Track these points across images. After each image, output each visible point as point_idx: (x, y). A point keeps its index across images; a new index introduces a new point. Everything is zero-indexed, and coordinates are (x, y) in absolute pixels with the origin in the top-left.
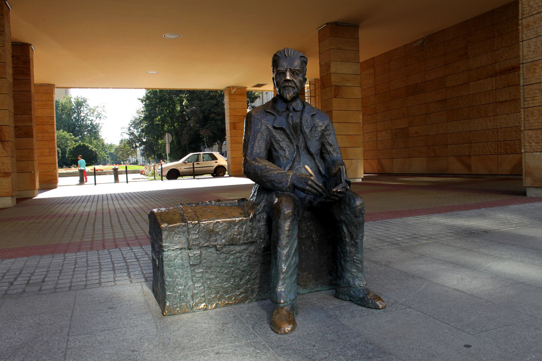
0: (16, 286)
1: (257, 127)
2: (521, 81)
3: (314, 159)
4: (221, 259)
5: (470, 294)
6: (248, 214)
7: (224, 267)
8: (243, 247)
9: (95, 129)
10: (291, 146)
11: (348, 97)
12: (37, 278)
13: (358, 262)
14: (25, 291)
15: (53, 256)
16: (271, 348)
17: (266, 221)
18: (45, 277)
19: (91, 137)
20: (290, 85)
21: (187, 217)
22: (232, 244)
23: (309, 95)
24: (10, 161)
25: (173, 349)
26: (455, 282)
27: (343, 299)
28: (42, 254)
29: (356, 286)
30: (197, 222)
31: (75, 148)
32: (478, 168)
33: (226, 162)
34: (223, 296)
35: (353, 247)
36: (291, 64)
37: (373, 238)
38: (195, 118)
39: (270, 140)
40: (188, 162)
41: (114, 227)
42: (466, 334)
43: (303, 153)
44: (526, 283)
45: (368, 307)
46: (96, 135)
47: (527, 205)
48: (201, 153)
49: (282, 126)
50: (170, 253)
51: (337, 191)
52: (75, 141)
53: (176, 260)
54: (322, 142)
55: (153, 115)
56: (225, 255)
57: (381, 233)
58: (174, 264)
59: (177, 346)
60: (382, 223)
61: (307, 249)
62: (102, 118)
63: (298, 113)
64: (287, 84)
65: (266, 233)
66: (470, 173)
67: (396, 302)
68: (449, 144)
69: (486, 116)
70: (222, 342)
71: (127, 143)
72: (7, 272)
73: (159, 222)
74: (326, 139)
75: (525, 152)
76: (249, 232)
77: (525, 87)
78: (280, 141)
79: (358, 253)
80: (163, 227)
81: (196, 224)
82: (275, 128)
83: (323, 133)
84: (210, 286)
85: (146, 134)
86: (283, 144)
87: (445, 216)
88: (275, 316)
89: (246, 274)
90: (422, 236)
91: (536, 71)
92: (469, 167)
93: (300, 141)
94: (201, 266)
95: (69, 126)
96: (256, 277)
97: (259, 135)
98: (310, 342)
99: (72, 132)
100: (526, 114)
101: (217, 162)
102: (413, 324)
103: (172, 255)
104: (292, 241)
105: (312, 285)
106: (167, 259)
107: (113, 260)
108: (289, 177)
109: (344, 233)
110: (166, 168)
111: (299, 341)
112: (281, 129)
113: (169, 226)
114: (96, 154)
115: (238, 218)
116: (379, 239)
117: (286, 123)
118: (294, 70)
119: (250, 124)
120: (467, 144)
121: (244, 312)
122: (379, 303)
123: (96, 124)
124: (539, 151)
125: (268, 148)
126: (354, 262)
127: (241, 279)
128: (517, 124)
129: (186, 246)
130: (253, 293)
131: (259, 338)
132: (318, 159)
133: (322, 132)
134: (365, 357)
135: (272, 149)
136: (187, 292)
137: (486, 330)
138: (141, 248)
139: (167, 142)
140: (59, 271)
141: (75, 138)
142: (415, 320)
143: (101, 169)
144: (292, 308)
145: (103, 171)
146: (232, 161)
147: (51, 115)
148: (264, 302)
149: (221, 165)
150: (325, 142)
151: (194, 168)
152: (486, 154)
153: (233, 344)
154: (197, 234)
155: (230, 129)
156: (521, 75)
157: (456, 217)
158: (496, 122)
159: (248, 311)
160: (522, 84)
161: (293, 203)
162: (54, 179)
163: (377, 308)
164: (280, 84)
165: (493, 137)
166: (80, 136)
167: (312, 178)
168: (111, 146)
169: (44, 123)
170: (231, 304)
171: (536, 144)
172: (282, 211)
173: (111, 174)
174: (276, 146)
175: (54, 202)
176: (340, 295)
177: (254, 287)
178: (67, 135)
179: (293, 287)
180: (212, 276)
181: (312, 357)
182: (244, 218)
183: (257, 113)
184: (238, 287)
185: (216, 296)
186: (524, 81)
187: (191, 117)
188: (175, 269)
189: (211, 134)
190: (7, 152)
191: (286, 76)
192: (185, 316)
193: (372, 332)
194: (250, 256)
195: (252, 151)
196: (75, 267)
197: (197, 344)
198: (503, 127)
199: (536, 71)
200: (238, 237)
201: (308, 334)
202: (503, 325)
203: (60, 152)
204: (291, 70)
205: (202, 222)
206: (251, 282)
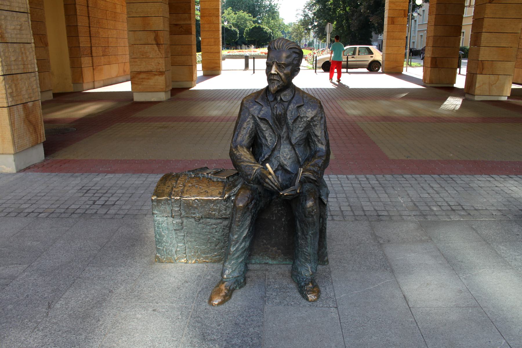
8: (219, 221)
11: (508, 2)
20: (275, 78)
24: (164, 61)
29: (302, 273)
30: (178, 198)
35: (303, 240)
38: (366, 3)
53: (163, 224)
58: (162, 227)
61: (277, 229)
72: (100, 189)
74: (312, 129)
76: (223, 210)
78: (264, 131)
85: (317, 17)
89: (220, 241)
95: (249, 7)
105: (281, 258)
109: (298, 227)
110: (320, 60)
114: (270, 35)
118: (280, 64)
123: (275, 4)
125: (253, 135)
126: (304, 254)
127: (216, 246)
139: (328, 32)
141: (253, 19)
146: (387, 57)
147: (217, 8)
149: (376, 60)
150: (311, 133)
151: (347, 61)
162: (218, 67)
169: (211, 15)
170: (207, 262)
179: (239, 266)
180: (193, 240)
182: (220, 198)
188: (163, 231)
190: (161, 54)
192: (168, 265)
195: (237, 139)
200: (213, 213)
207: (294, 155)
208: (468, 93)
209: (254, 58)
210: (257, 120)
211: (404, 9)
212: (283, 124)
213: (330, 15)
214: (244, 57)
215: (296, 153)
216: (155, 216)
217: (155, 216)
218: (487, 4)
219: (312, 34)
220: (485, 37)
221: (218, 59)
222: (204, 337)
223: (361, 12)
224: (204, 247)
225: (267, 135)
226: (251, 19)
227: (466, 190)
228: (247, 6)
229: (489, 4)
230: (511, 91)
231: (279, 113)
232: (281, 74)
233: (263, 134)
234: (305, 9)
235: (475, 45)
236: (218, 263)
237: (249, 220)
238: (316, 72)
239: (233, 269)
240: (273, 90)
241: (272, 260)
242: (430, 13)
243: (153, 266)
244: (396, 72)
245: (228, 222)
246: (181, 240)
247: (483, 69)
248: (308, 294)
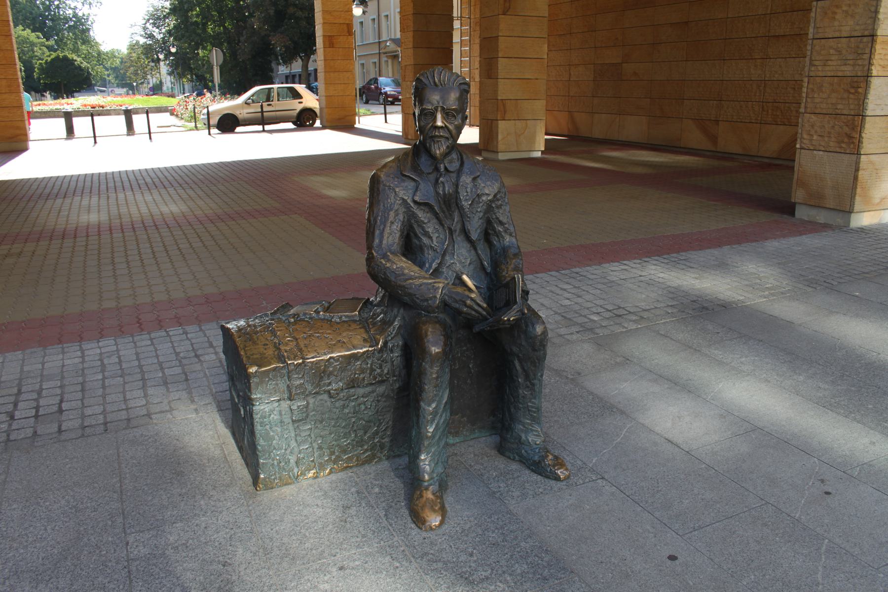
0: (20, 421)
1: (389, 201)
2: (811, 30)
3: (475, 249)
4: (337, 408)
5: (687, 450)
6: (375, 340)
7: (341, 418)
8: (369, 389)
9: (82, 24)
10: (441, 230)
11: (526, 14)
12: (49, 403)
13: (534, 410)
14: (36, 432)
15: (63, 348)
16: (414, 557)
17: (402, 350)
18: (61, 401)
19: (75, 39)
20: (441, 134)
21: (286, 352)
23: (459, 16)
25: (279, 560)
26: (669, 425)
27: (510, 459)
28: (44, 343)
29: (530, 443)
30: (301, 361)
31: (50, 62)
32: (729, 143)
33: (318, 103)
34: (340, 457)
35: (527, 389)
36: (444, 99)
37: (556, 313)
39: (409, 220)
40: (253, 102)
41: (129, 205)
42: (673, 533)
43: (459, 239)
44: (765, 429)
45: (545, 477)
46: (85, 36)
47: (792, 240)
48: (275, 86)
49: (426, 200)
50: (262, 408)
52: (50, 48)
53: (272, 416)
54: (488, 217)
55: (186, 6)
56: (342, 402)
57: (567, 302)
58: (270, 422)
59: (284, 554)
60: (571, 277)
62: (94, 5)
63: (452, 175)
64: (436, 134)
65: (402, 367)
66: (715, 150)
67: (584, 466)
68: (685, 98)
69: (750, 58)
70: (346, 546)
71: (142, 53)
73: (245, 362)
75: (802, 148)
76: (377, 367)
77: (815, 41)
78: (425, 223)
79: (535, 398)
80: (252, 373)
81: (300, 364)
82: (415, 202)
83: (490, 205)
84: (321, 446)
85: (175, 39)
86: (429, 227)
87: (667, 263)
88: (417, 500)
90: (630, 312)
91: (837, 17)
92: (714, 139)
93: (454, 221)
94: (308, 420)
95: (34, 19)
96: (387, 427)
97: (392, 214)
98: (465, 546)
99: (41, 31)
100: (811, 86)
101: (301, 103)
102: (605, 513)
103: (265, 410)
104: (441, 391)
106: (259, 416)
107: (161, 359)
108: (438, 292)
109: (517, 370)
110: (215, 112)
111: (452, 544)
112: (426, 204)
113: (260, 370)
114: (88, 73)
115: (361, 349)
116: (565, 317)
117: (433, 194)
118: (448, 109)
119: (378, 195)
120: (715, 102)
121: (372, 483)
122: (561, 472)
123: (84, 15)
124: (823, 149)
125: (405, 233)
126: (529, 410)
127: (365, 433)
128: (797, 77)
129: (286, 396)
130: (382, 449)
131: (396, 537)
132: (482, 247)
134: (539, 578)
135: (412, 234)
136: (290, 457)
137: (700, 528)
138: (201, 330)
139: (215, 64)
140: (79, 387)
141: (47, 43)
142: (608, 505)
143: (102, 104)
144: (440, 485)
145: (105, 109)
146: (329, 102)
147: (4, 18)
148: (398, 461)
149: (308, 107)
150: (493, 219)
151: (262, 112)
152: (743, 121)
153: (361, 550)
154: (301, 378)
155: (324, 48)
156: (812, 20)
157: (684, 267)
158: (764, 69)
159: (376, 480)
160: (810, 36)
161: (444, 336)
163: (557, 478)
164: (426, 131)
165: (758, 94)
166: (56, 38)
167: (473, 296)
168: (112, 55)
170: (351, 467)
171: (819, 138)
172: (427, 350)
173: (119, 114)
174: (418, 231)
175: (31, 192)
176: (507, 453)
177: (383, 441)
178: (33, 36)
181: (469, 576)
182: (370, 349)
183: (389, 176)
184: (360, 443)
185: (330, 459)
186: (815, 30)
187: (254, 12)
188: (271, 428)
189: (290, 42)
191: (435, 119)
192: (287, 490)
193: (549, 528)
194: (378, 401)
195: (381, 242)
196: (104, 378)
197: (311, 549)
198: (775, 79)
199: (837, 17)
200: (362, 376)
201: (463, 531)
202: (723, 516)
203: (23, 68)
204: (443, 109)
205: (309, 361)
206: (380, 434)
207: (475, 258)
208: (487, 150)
209: (147, 113)
210: (411, 207)
211: (347, 22)
212: (453, 209)
213: (199, 35)
214: (63, 114)
215: (478, 255)
216: (258, 404)
217: (258, 404)
218: (500, 16)
219: (164, 68)
220: (503, 65)
221: (20, 119)
222: (466, 578)
223: (254, 29)
224: (345, 441)
225: (430, 230)
226: (42, 42)
227: (610, 287)
228: (26, 18)
229: (503, 16)
230: (545, 142)
231: (449, 192)
232: (451, 127)
233: (423, 229)
234: (146, 23)
235: (490, 77)
236: (369, 464)
238: (210, 134)
239: (436, 462)
240: (440, 154)
241: (453, 437)
242: (404, 29)
243: (258, 498)
244: (345, 124)
245: (384, 387)
246: (306, 437)
247: (505, 112)
248: (556, 470)
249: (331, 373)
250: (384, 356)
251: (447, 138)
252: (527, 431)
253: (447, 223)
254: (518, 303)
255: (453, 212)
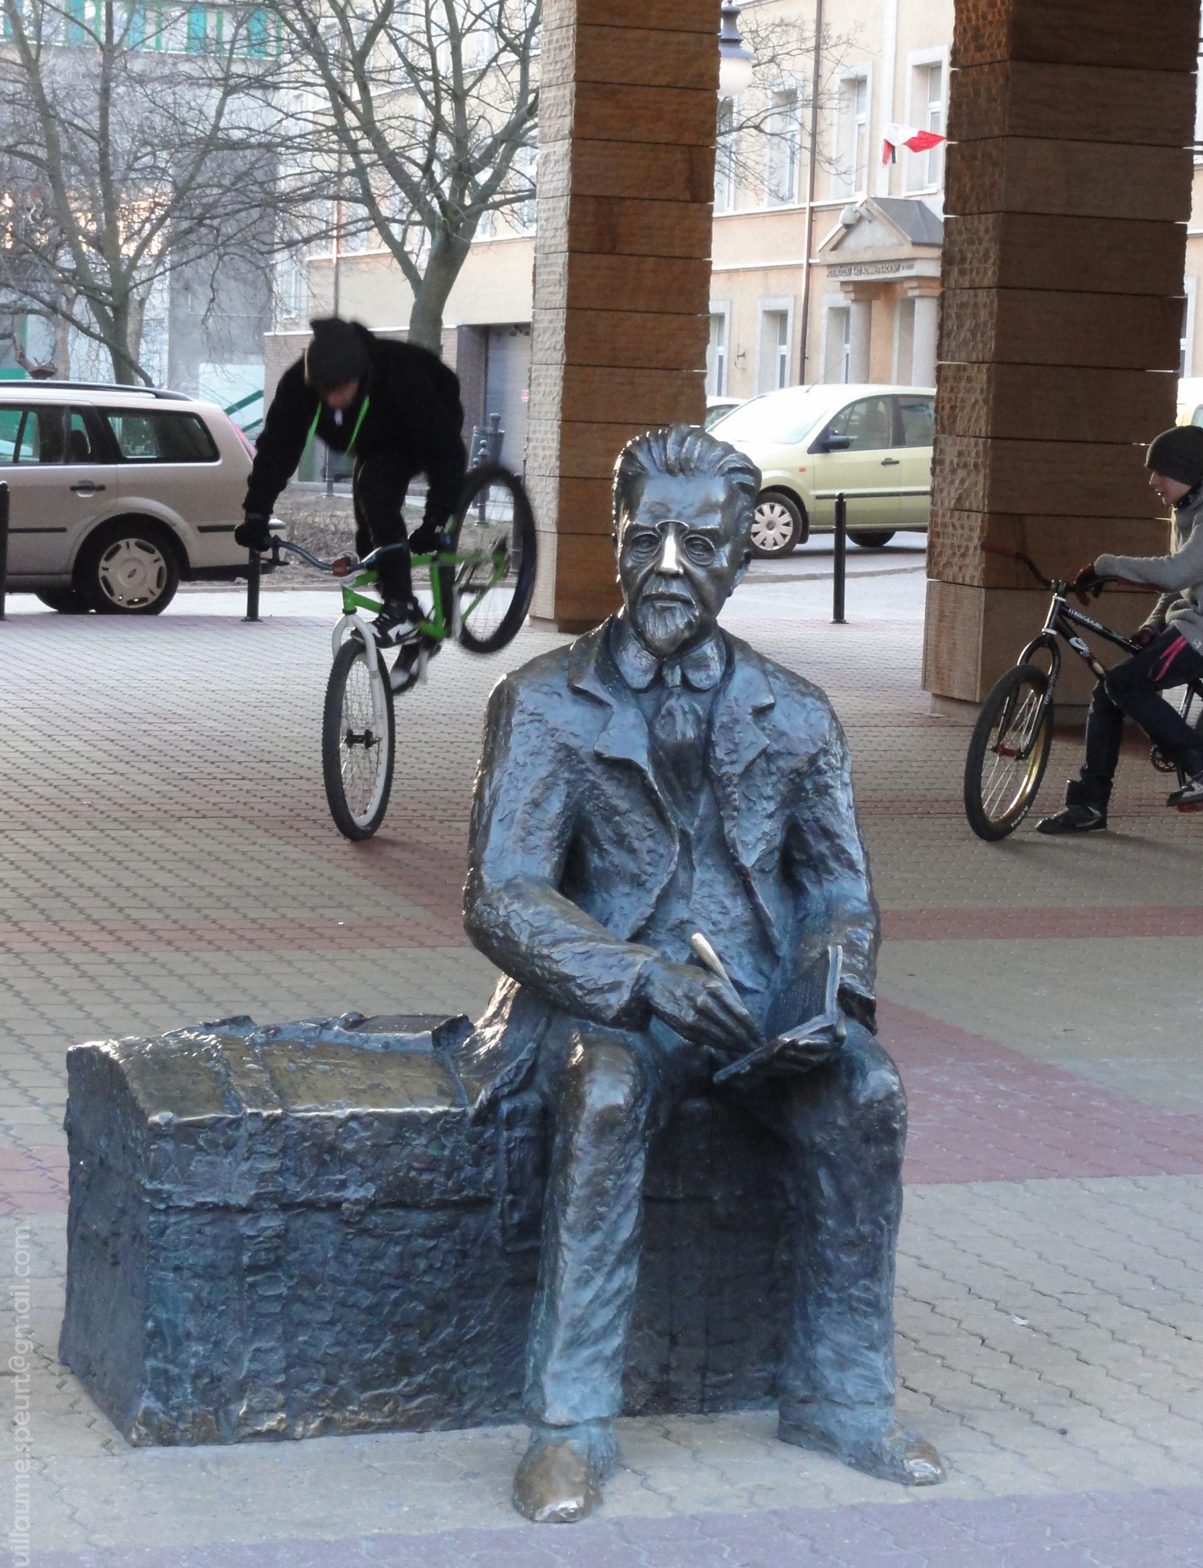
8: (441, 1217)
22: (401, 1205)
51: (793, 1044)
76: (465, 1161)
127: (425, 1338)
132: (767, 896)
133: (792, 780)
135: (586, 841)
150: (806, 821)
161: (634, 1075)
174: (603, 831)
191: (660, 554)
200: (426, 1177)
204: (680, 530)
207: (747, 916)
232: (700, 574)
237: (638, 1171)
249: (350, 1158)
250: (487, 1135)
251: (686, 602)
252: (843, 1362)
253: (678, 820)
254: (828, 1013)
255: (697, 791)
